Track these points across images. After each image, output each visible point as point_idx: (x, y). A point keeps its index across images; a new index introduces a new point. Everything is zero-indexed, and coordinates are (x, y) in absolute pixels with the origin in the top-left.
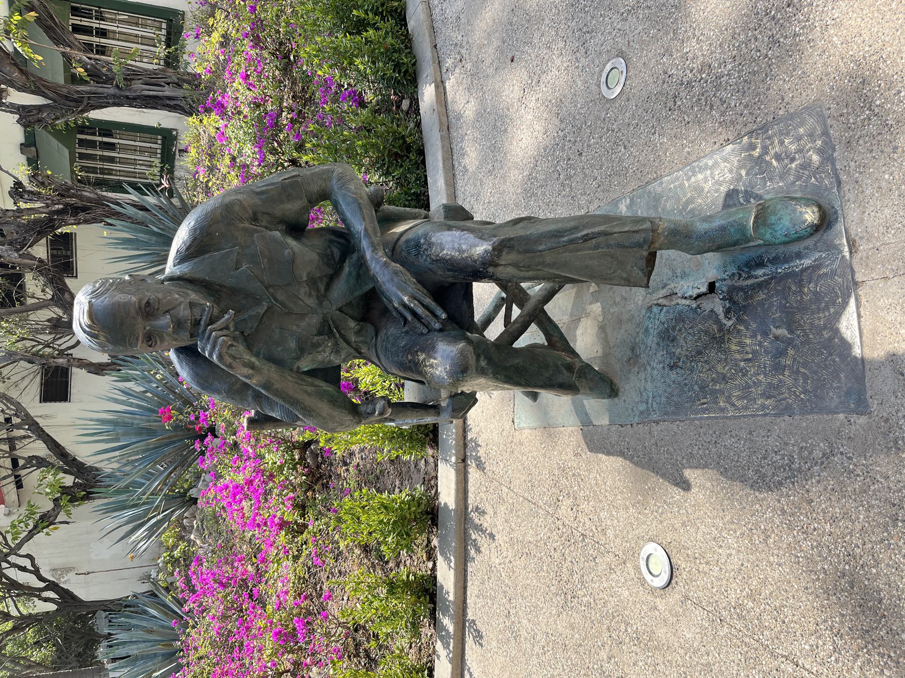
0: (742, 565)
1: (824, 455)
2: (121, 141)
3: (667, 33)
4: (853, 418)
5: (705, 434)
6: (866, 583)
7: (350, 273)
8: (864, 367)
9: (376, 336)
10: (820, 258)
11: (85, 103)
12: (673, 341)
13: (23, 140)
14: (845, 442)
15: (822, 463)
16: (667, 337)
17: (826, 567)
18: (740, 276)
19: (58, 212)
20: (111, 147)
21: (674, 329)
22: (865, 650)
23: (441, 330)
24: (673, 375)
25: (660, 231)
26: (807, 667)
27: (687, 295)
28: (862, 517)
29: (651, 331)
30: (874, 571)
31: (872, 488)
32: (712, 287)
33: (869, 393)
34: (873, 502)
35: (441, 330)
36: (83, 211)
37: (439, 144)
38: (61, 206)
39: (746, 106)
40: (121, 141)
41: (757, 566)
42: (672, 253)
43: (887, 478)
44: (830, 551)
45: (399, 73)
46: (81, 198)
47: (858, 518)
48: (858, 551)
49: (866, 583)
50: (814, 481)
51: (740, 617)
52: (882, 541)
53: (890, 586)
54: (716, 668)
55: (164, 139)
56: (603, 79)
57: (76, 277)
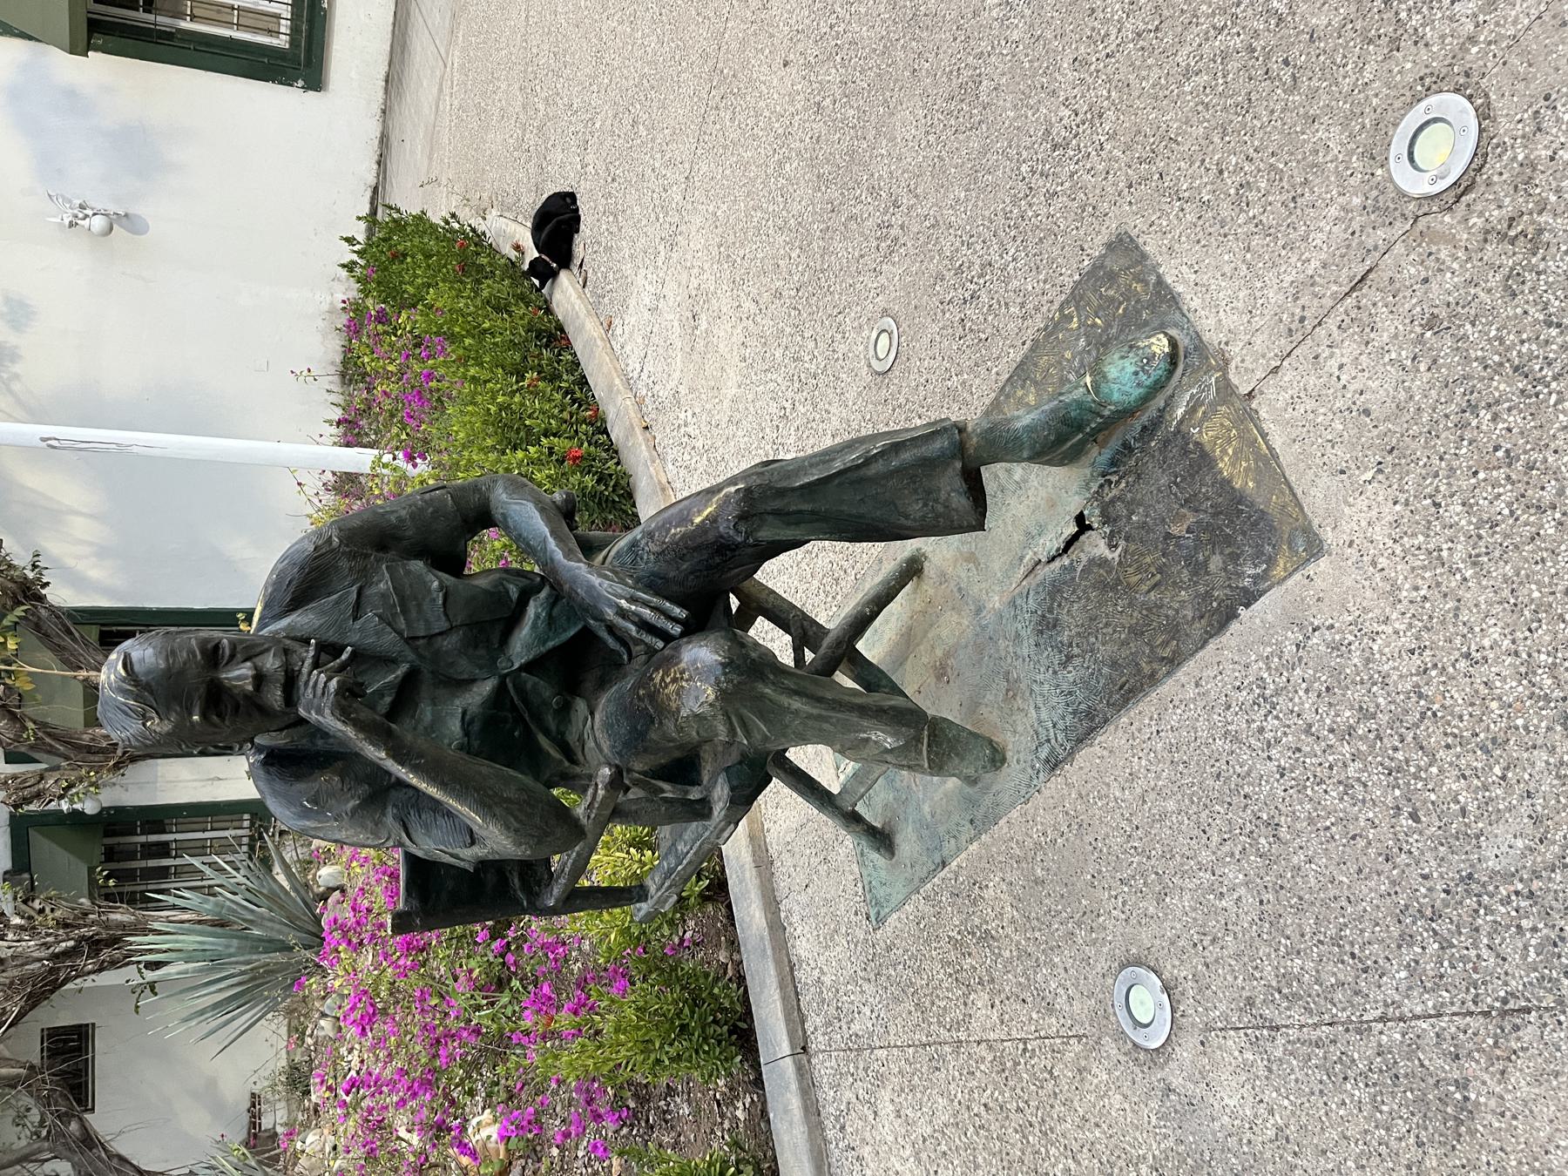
0: (1261, 902)
1: (1298, 646)
2: (179, 836)
3: (932, 258)
4: (1311, 569)
5: (1140, 730)
6: (1433, 797)
7: (537, 616)
8: (1294, 495)
9: (592, 714)
10: (1192, 396)
11: (119, 752)
12: (1055, 626)
13: (8, 865)
14: (1314, 610)
15: (1300, 659)
16: (1047, 625)
17: (1371, 815)
18: (1110, 482)
19: (66, 954)
20: (163, 850)
21: (1050, 611)
22: (1482, 912)
23: (683, 635)
24: (1071, 674)
25: (969, 429)
26: (1418, 1010)
27: (1053, 552)
28: (1381, 700)
29: (1023, 633)
30: (1434, 770)
31: (1375, 648)
32: (1082, 524)
33: (1316, 522)
34: (1386, 667)
35: (683, 635)
36: (108, 946)
37: (776, 995)
38: (71, 943)
39: (1045, 282)
40: (179, 836)
41: (1282, 887)
42: (999, 468)
43: (1387, 621)
44: (1365, 786)
45: (607, 486)
46: (107, 925)
47: (1378, 706)
48: (1400, 755)
49: (1433, 797)
50: (1301, 693)
51: (1293, 998)
52: (1423, 714)
53: (1465, 777)
54: (1292, 1131)
55: (254, 816)
56: (872, 352)
57: (93, 1109)
